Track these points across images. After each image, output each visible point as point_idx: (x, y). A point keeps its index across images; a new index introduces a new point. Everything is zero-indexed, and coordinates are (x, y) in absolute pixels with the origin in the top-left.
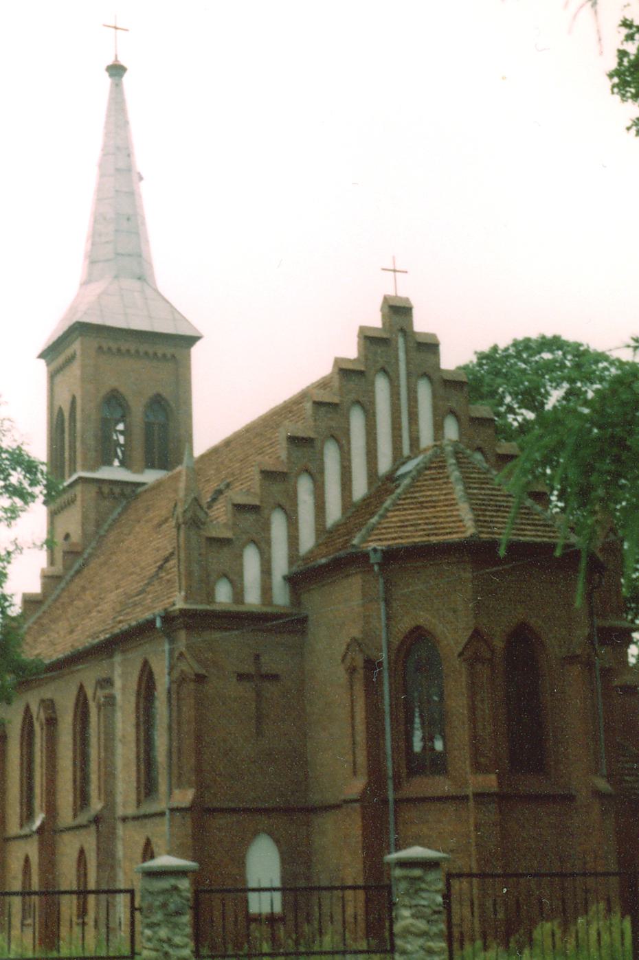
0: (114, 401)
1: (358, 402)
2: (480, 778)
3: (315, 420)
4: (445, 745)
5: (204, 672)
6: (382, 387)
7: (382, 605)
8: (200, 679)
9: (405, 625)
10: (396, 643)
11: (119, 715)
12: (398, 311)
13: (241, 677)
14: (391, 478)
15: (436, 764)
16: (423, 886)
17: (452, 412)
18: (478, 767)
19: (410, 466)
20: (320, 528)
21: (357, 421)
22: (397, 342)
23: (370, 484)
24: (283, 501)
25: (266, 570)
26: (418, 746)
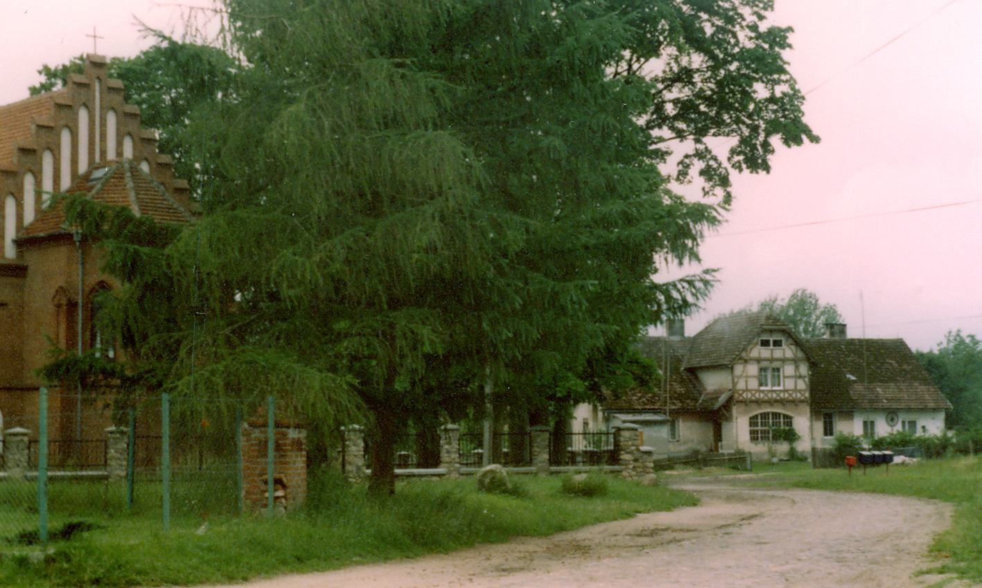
1: (67, 126)
3: (37, 137)
4: (115, 355)
6: (83, 115)
7: (80, 266)
10: (87, 289)
14: (87, 177)
17: (130, 134)
19: (98, 174)
20: (38, 211)
21: (65, 138)
22: (94, 86)
23: (73, 180)
24: (13, 190)
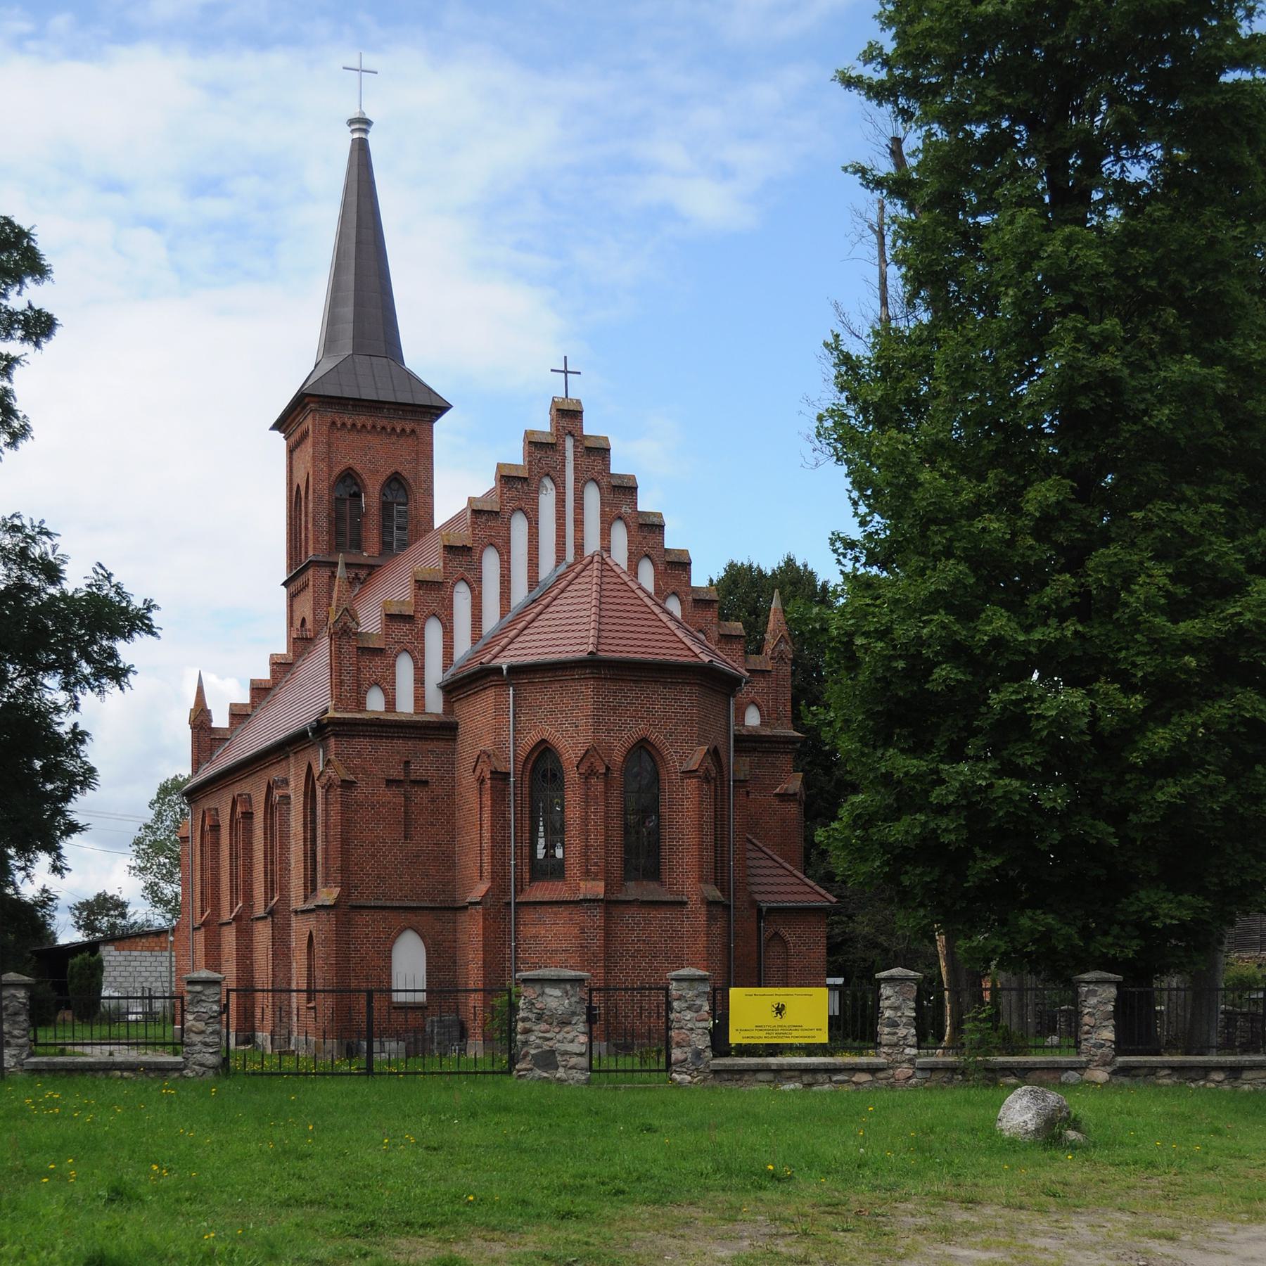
0: (349, 481)
2: (590, 884)
5: (352, 778)
8: (347, 785)
9: (531, 738)
11: (293, 813)
12: (568, 414)
13: (390, 783)
15: (553, 870)
16: (203, 998)
18: (587, 874)
25: (419, 680)
26: (541, 853)
